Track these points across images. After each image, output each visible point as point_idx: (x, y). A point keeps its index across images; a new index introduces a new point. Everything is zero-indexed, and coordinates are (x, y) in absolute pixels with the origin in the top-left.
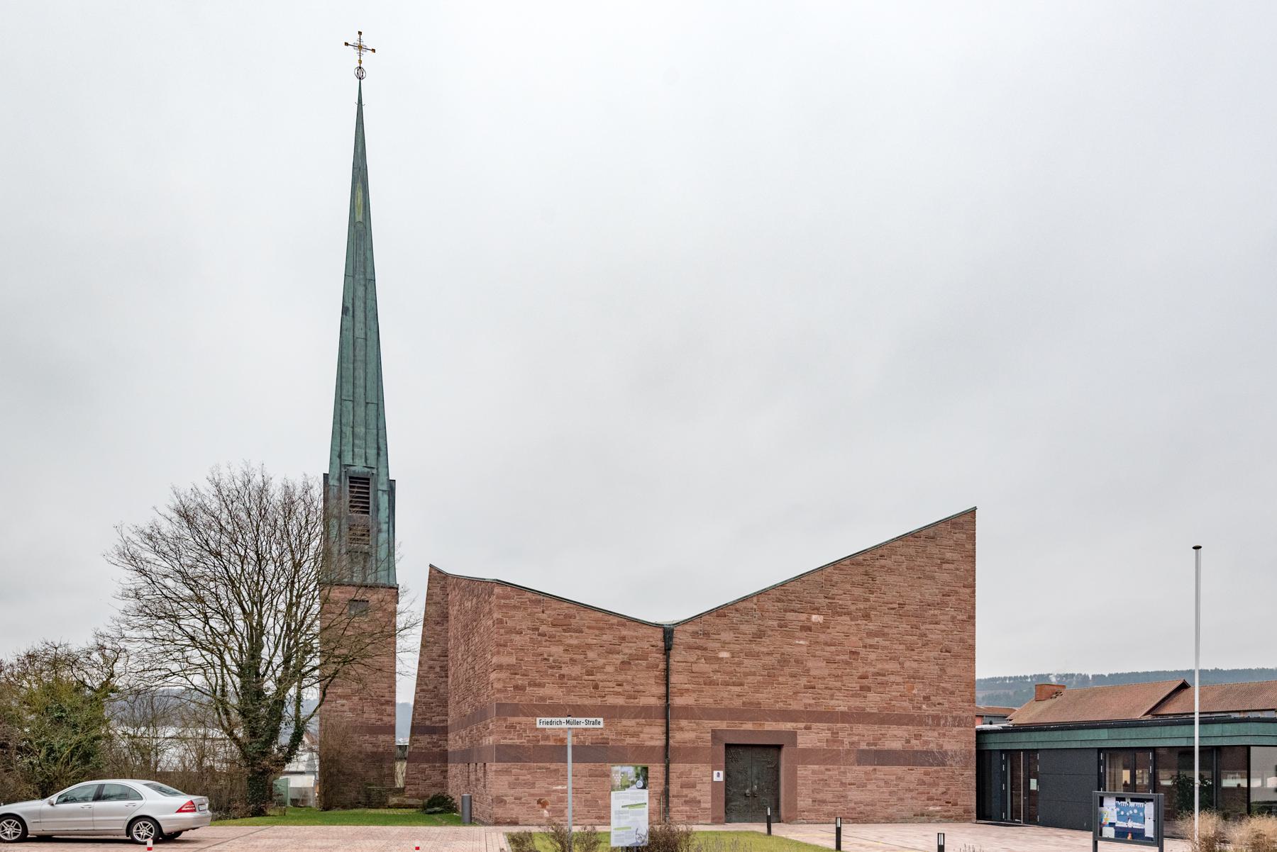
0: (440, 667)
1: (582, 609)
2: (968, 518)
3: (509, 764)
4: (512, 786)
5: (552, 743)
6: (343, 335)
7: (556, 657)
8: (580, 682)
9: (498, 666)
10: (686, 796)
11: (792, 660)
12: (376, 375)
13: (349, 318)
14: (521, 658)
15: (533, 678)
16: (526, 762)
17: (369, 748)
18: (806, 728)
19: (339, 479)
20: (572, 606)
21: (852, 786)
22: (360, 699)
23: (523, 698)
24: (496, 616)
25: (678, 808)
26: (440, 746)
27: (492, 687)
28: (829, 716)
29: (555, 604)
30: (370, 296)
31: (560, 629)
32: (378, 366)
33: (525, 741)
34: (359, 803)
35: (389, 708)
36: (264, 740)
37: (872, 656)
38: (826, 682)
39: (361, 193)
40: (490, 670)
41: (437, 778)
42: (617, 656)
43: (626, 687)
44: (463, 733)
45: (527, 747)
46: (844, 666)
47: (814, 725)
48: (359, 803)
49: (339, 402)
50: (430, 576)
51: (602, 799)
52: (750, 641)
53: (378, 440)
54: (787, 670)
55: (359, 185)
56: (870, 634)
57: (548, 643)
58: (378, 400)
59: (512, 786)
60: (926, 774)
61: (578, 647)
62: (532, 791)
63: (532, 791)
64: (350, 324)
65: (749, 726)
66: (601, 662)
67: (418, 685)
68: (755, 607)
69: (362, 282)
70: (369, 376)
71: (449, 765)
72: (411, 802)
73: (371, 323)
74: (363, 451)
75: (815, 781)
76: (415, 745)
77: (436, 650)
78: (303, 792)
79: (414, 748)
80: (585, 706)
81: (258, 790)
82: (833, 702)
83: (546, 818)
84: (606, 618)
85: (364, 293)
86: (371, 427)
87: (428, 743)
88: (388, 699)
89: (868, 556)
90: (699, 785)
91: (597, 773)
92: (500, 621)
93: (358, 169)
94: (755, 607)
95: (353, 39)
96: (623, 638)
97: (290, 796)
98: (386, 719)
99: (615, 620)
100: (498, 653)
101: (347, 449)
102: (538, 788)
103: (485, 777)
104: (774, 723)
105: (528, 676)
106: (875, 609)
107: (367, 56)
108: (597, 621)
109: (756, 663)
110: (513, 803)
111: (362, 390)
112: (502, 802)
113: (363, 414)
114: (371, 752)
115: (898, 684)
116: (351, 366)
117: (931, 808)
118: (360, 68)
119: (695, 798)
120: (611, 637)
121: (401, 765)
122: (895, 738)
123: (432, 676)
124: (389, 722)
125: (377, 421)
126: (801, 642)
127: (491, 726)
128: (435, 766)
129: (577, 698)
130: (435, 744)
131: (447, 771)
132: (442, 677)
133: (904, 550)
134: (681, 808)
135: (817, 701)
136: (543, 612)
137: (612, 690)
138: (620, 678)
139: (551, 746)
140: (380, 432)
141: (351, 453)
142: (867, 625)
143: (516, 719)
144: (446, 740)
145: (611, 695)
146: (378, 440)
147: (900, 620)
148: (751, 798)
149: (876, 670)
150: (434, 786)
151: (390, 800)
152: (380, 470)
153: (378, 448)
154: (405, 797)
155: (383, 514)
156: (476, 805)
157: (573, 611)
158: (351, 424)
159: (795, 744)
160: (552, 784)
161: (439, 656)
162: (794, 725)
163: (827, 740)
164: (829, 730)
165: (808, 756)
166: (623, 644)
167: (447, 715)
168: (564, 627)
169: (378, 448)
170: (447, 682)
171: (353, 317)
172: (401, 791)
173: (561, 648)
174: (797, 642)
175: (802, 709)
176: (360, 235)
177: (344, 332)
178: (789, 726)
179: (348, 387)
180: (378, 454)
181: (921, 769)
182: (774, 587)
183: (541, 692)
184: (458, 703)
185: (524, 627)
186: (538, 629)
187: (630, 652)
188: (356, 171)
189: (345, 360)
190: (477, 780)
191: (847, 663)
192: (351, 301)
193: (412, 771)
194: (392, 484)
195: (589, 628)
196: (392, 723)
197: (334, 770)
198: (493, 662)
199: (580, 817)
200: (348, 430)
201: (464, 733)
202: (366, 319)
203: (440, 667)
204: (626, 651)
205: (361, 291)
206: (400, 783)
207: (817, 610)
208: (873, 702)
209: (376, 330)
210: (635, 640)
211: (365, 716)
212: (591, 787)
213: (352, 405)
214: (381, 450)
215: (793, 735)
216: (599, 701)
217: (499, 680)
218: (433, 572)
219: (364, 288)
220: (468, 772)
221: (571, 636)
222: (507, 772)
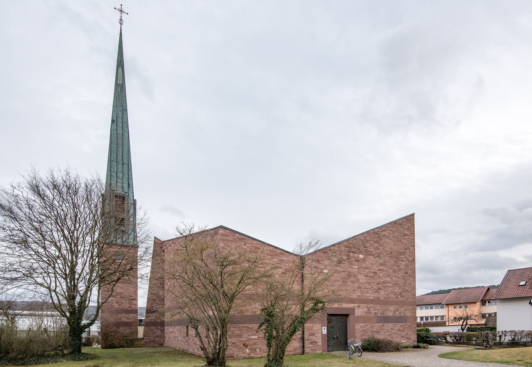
2: (412, 217)
6: (112, 132)
10: (311, 340)
11: (353, 275)
16: (237, 324)
18: (358, 307)
20: (259, 242)
21: (375, 333)
22: (121, 297)
25: (308, 346)
26: (160, 319)
28: (366, 301)
29: (250, 241)
30: (125, 117)
32: (128, 148)
35: (134, 302)
37: (382, 274)
38: (365, 285)
41: (159, 333)
42: (279, 270)
46: (372, 279)
47: (361, 305)
52: (336, 265)
53: (128, 180)
54: (351, 280)
55: (120, 69)
56: (381, 265)
58: (128, 162)
60: (401, 326)
62: (241, 339)
63: (241, 339)
64: (115, 128)
65: (336, 305)
68: (338, 249)
73: (125, 129)
75: (362, 331)
76: (148, 318)
79: (148, 320)
82: (368, 295)
84: (275, 250)
86: (125, 174)
88: (134, 297)
89: (379, 230)
90: (317, 334)
94: (338, 249)
95: (119, 7)
96: (283, 260)
98: (133, 307)
99: (279, 251)
104: (346, 304)
106: (382, 254)
107: (124, 15)
109: (338, 275)
111: (121, 158)
113: (122, 168)
115: (391, 287)
117: (403, 341)
118: (121, 19)
119: (315, 340)
120: (277, 260)
122: (390, 311)
124: (135, 308)
125: (128, 172)
126: (356, 267)
131: (164, 330)
133: (391, 228)
134: (310, 345)
135: (362, 294)
136: (245, 245)
139: (250, 315)
140: (130, 177)
142: (379, 260)
146: (128, 180)
147: (391, 259)
148: (336, 340)
149: (383, 281)
150: (157, 337)
152: (130, 194)
153: (129, 184)
157: (259, 246)
158: (116, 172)
159: (354, 314)
160: (250, 335)
162: (354, 305)
163: (366, 312)
164: (366, 307)
165: (359, 319)
169: (129, 184)
171: (117, 124)
174: (354, 267)
175: (356, 297)
177: (112, 131)
178: (352, 305)
179: (114, 155)
180: (129, 187)
181: (399, 324)
182: (345, 241)
189: (113, 143)
191: (373, 277)
192: (116, 117)
194: (135, 201)
200: (114, 174)
202: (123, 127)
203: (160, 283)
205: (120, 115)
207: (361, 252)
208: (382, 294)
209: (128, 132)
211: (123, 305)
213: (116, 164)
214: (130, 185)
215: (353, 309)
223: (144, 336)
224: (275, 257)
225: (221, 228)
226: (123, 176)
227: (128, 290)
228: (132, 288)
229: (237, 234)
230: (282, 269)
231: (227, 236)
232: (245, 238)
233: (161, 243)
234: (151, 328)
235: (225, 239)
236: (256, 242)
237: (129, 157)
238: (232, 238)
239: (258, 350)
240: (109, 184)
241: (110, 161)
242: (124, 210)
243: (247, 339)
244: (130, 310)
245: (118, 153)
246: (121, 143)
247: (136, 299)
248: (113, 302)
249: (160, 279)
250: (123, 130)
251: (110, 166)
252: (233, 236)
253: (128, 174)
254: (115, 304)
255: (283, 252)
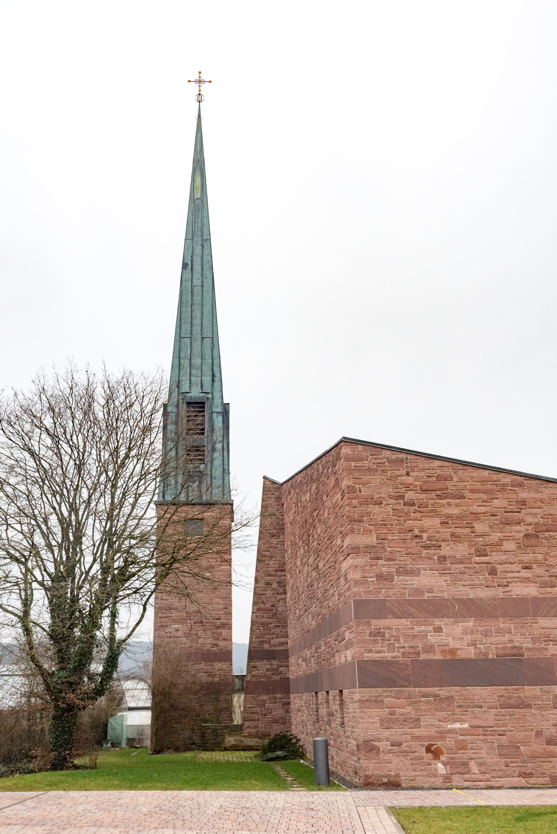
0: (278, 583)
1: (460, 467)
3: (380, 690)
4: (386, 724)
5: (438, 656)
7: (431, 532)
8: (469, 566)
9: (352, 549)
12: (211, 313)
13: (188, 271)
14: (383, 536)
15: (403, 563)
16: (404, 686)
17: (204, 678)
19: (177, 406)
20: (446, 464)
23: (391, 592)
24: (345, 483)
27: (346, 579)
29: (422, 463)
30: (206, 252)
31: (433, 494)
33: (400, 654)
34: (194, 744)
35: (224, 632)
36: (72, 667)
39: (200, 178)
40: (342, 558)
42: (518, 528)
43: (538, 570)
44: (307, 653)
45: (404, 663)
48: (194, 744)
49: (178, 339)
50: (263, 488)
51: (525, 743)
53: (212, 368)
55: (198, 173)
57: (418, 515)
58: (213, 334)
59: (386, 724)
61: (460, 517)
62: (417, 732)
63: (417, 732)
66: (495, 536)
67: (255, 604)
69: (200, 242)
70: (205, 315)
71: (292, 696)
72: (249, 742)
73: (207, 273)
74: (200, 379)
76: (253, 673)
77: (273, 564)
78: (140, 729)
80: (481, 600)
81: (63, 731)
83: (441, 775)
84: (495, 476)
85: (201, 250)
86: (207, 357)
87: (268, 670)
91: (512, 701)
92: (351, 489)
93: (197, 162)
95: (196, 77)
96: (523, 502)
97: (127, 734)
98: (222, 644)
100: (352, 531)
101: (185, 380)
102: (424, 727)
103: (342, 709)
105: (395, 560)
107: (204, 86)
108: (482, 481)
110: (390, 752)
111: (199, 328)
112: (373, 749)
113: (200, 347)
114: (206, 683)
116: (189, 309)
118: (200, 94)
121: (239, 697)
123: (269, 593)
127: (347, 635)
128: (275, 698)
129: (467, 588)
130: (275, 672)
132: (280, 594)
136: (408, 474)
137: (517, 575)
138: (527, 558)
141: (188, 382)
143: (383, 623)
144: (287, 666)
145: (516, 582)
146: (212, 368)
150: (275, 721)
151: (227, 740)
152: (214, 394)
153: (213, 375)
154: (244, 737)
155: (218, 434)
156: (332, 751)
158: (189, 357)
160: (446, 720)
161: (276, 571)
166: (523, 511)
167: (287, 636)
168: (438, 493)
169: (213, 375)
170: (285, 599)
171: (192, 270)
172: (240, 728)
173: (438, 521)
176: (199, 209)
177: (184, 283)
179: (186, 327)
180: (213, 381)
183: (415, 582)
184: (299, 619)
185: (383, 495)
186: (402, 497)
187: (536, 520)
188: (195, 163)
189: (184, 305)
190: (330, 714)
192: (190, 258)
193: (250, 704)
195: (471, 491)
196: (228, 649)
197: (166, 705)
198: (345, 546)
199: (494, 774)
200: (185, 363)
201: (308, 652)
203: (278, 583)
204: (530, 519)
206: (237, 719)
210: (540, 504)
211: (200, 641)
212: (505, 725)
216: (499, 593)
217: (356, 567)
218: (267, 483)
219: (201, 247)
220: (317, 704)
221: (449, 504)
222: (377, 702)
223: (243, 721)
224: (499, 495)
225: (342, 444)
226: (202, 363)
227: (211, 604)
228: (219, 598)
229: (384, 451)
230: (525, 525)
231: (361, 459)
232: (407, 458)
233: (278, 488)
234: (259, 698)
235: (355, 466)
236: (437, 463)
237: (215, 324)
238: (373, 463)
239: (474, 768)
240: (176, 384)
241: (179, 338)
242: (203, 429)
243: (437, 732)
244: (215, 654)
245: (193, 321)
246: (200, 301)
247: (228, 626)
248: (179, 633)
249: (279, 572)
250: (202, 277)
251: (178, 348)
252: (376, 457)
253: (212, 356)
254: (184, 640)
255: (522, 478)
